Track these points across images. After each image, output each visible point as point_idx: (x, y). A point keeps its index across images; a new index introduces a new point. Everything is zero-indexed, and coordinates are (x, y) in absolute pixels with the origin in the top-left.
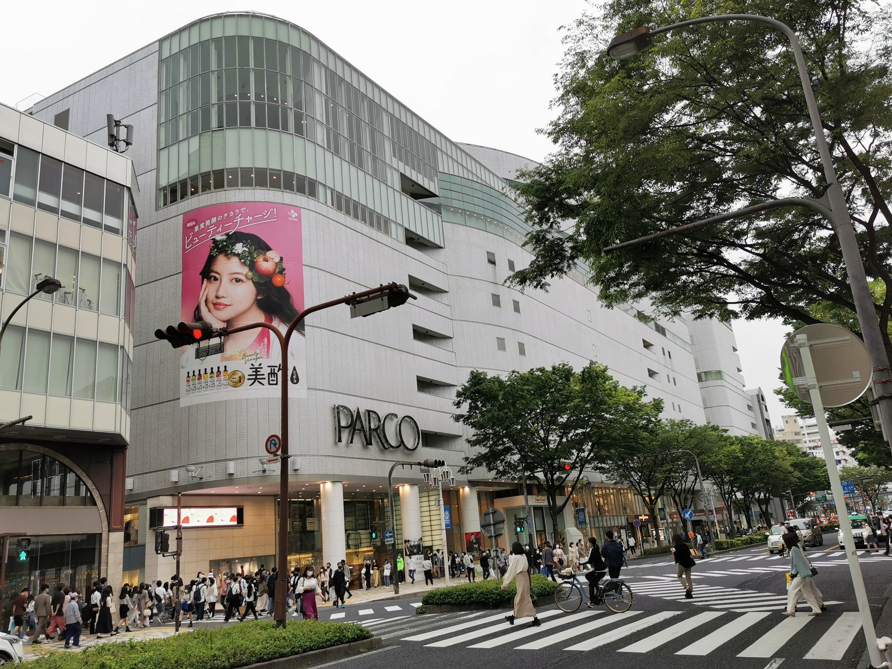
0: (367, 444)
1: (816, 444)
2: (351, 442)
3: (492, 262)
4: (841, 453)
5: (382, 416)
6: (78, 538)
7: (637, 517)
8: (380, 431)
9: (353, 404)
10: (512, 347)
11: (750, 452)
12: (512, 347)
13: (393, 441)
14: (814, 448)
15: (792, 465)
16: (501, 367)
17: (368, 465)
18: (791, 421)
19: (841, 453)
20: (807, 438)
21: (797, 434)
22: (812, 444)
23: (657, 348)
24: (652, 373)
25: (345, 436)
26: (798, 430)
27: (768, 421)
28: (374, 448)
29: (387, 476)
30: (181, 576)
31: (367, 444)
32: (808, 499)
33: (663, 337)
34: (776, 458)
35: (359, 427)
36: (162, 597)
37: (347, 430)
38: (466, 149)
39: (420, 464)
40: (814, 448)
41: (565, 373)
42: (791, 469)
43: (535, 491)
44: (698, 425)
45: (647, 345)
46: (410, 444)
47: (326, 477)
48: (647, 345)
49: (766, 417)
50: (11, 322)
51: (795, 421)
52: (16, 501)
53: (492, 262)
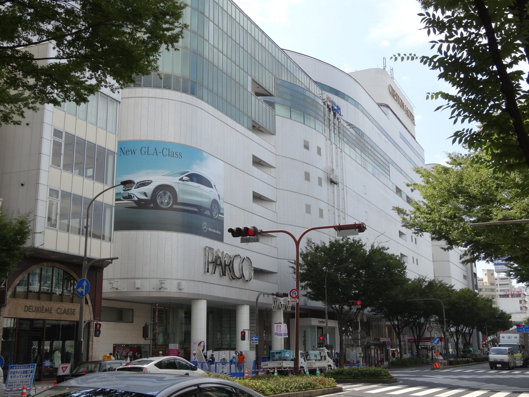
0: (223, 275)
2: (214, 273)
3: (307, 147)
6: (67, 323)
10: (315, 211)
12: (315, 211)
13: (238, 274)
20: (499, 288)
25: (211, 267)
27: (475, 274)
28: (226, 278)
29: (255, 301)
31: (223, 275)
33: (400, 198)
37: (212, 264)
38: (289, 54)
39: (273, 294)
44: (501, 308)
46: (247, 277)
49: (474, 271)
50: (97, 199)
53: (307, 147)
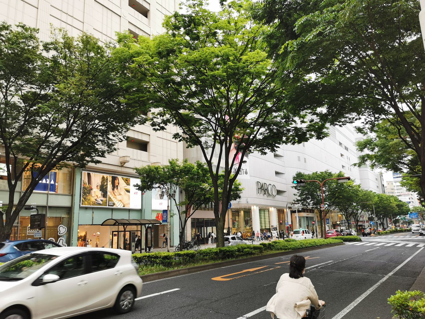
1: (400, 194)
4: (411, 199)
5: (268, 184)
7: (336, 222)
8: (267, 190)
9: (262, 181)
11: (380, 200)
14: (399, 196)
15: (396, 205)
16: (309, 170)
17: (264, 200)
18: (390, 184)
19: (411, 199)
20: (396, 191)
21: (392, 189)
22: (398, 194)
23: (345, 156)
24: (343, 167)
26: (393, 188)
27: (383, 185)
30: (111, 236)
32: (397, 218)
34: (391, 203)
35: (263, 189)
36: (256, 234)
40: (399, 196)
41: (330, 175)
42: (396, 207)
43: (309, 211)
45: (342, 155)
47: (254, 205)
48: (342, 155)
51: (392, 184)
52: (205, 209)
